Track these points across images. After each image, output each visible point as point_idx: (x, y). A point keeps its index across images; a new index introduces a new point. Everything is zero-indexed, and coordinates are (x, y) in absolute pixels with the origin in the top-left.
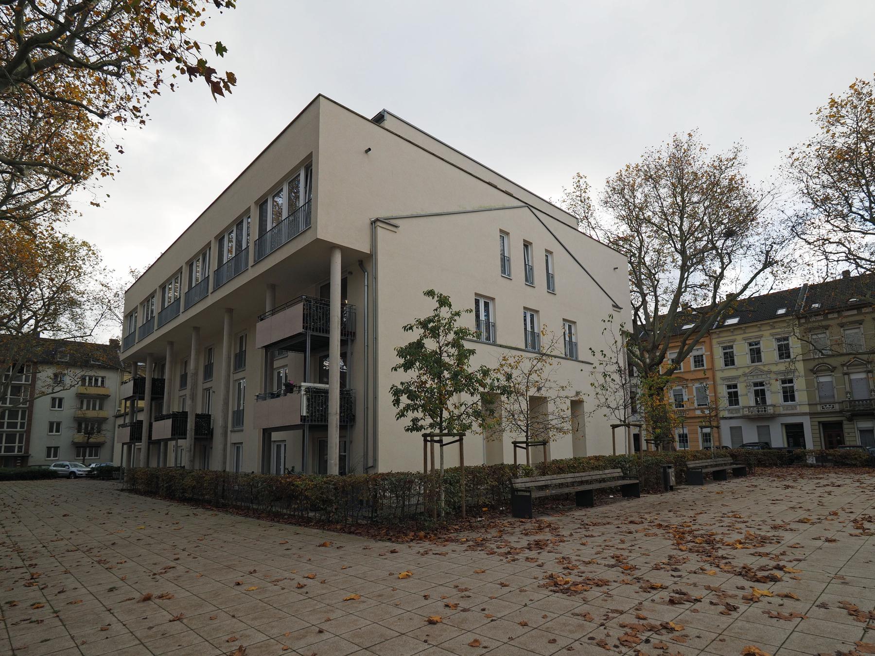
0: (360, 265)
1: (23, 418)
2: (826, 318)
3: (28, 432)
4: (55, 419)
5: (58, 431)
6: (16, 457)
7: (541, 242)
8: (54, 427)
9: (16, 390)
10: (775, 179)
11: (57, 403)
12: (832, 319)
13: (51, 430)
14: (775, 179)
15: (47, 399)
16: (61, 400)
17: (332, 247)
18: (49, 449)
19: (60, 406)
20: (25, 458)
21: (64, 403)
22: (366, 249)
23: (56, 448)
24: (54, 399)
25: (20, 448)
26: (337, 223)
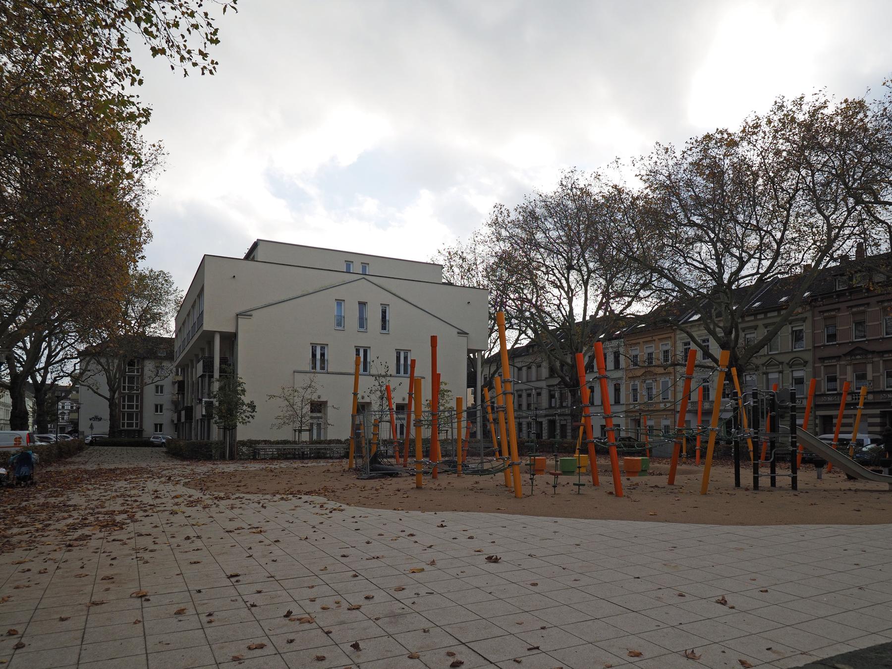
0: (230, 340)
1: (137, 401)
2: (756, 319)
3: (141, 412)
4: (363, 343)
5: (161, 411)
6: (134, 431)
7: (375, 300)
8: (158, 408)
9: (131, 380)
10: (874, 109)
11: (159, 389)
12: (748, 321)
13: (157, 411)
14: (874, 109)
15: (153, 386)
16: (162, 387)
17: (212, 334)
18: (156, 425)
19: (162, 392)
20: (140, 432)
21: (165, 389)
22: (233, 330)
23: (161, 425)
24: (157, 387)
25: (137, 424)
26: (215, 321)
